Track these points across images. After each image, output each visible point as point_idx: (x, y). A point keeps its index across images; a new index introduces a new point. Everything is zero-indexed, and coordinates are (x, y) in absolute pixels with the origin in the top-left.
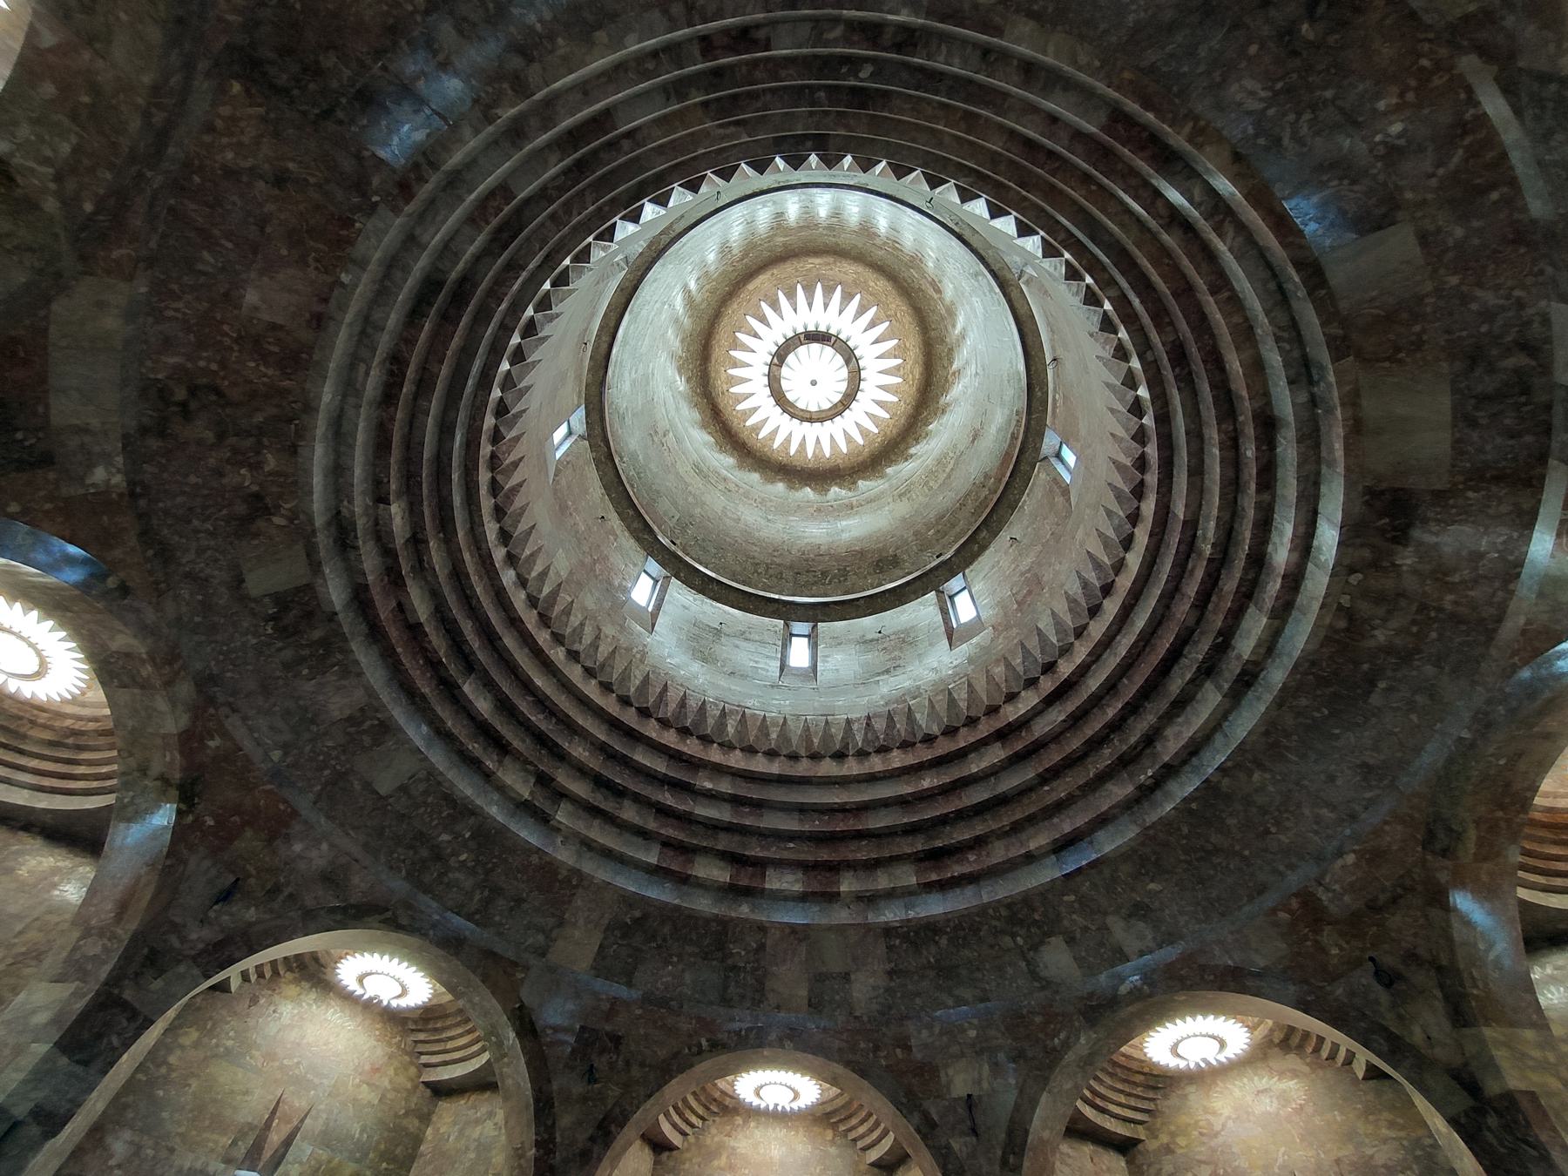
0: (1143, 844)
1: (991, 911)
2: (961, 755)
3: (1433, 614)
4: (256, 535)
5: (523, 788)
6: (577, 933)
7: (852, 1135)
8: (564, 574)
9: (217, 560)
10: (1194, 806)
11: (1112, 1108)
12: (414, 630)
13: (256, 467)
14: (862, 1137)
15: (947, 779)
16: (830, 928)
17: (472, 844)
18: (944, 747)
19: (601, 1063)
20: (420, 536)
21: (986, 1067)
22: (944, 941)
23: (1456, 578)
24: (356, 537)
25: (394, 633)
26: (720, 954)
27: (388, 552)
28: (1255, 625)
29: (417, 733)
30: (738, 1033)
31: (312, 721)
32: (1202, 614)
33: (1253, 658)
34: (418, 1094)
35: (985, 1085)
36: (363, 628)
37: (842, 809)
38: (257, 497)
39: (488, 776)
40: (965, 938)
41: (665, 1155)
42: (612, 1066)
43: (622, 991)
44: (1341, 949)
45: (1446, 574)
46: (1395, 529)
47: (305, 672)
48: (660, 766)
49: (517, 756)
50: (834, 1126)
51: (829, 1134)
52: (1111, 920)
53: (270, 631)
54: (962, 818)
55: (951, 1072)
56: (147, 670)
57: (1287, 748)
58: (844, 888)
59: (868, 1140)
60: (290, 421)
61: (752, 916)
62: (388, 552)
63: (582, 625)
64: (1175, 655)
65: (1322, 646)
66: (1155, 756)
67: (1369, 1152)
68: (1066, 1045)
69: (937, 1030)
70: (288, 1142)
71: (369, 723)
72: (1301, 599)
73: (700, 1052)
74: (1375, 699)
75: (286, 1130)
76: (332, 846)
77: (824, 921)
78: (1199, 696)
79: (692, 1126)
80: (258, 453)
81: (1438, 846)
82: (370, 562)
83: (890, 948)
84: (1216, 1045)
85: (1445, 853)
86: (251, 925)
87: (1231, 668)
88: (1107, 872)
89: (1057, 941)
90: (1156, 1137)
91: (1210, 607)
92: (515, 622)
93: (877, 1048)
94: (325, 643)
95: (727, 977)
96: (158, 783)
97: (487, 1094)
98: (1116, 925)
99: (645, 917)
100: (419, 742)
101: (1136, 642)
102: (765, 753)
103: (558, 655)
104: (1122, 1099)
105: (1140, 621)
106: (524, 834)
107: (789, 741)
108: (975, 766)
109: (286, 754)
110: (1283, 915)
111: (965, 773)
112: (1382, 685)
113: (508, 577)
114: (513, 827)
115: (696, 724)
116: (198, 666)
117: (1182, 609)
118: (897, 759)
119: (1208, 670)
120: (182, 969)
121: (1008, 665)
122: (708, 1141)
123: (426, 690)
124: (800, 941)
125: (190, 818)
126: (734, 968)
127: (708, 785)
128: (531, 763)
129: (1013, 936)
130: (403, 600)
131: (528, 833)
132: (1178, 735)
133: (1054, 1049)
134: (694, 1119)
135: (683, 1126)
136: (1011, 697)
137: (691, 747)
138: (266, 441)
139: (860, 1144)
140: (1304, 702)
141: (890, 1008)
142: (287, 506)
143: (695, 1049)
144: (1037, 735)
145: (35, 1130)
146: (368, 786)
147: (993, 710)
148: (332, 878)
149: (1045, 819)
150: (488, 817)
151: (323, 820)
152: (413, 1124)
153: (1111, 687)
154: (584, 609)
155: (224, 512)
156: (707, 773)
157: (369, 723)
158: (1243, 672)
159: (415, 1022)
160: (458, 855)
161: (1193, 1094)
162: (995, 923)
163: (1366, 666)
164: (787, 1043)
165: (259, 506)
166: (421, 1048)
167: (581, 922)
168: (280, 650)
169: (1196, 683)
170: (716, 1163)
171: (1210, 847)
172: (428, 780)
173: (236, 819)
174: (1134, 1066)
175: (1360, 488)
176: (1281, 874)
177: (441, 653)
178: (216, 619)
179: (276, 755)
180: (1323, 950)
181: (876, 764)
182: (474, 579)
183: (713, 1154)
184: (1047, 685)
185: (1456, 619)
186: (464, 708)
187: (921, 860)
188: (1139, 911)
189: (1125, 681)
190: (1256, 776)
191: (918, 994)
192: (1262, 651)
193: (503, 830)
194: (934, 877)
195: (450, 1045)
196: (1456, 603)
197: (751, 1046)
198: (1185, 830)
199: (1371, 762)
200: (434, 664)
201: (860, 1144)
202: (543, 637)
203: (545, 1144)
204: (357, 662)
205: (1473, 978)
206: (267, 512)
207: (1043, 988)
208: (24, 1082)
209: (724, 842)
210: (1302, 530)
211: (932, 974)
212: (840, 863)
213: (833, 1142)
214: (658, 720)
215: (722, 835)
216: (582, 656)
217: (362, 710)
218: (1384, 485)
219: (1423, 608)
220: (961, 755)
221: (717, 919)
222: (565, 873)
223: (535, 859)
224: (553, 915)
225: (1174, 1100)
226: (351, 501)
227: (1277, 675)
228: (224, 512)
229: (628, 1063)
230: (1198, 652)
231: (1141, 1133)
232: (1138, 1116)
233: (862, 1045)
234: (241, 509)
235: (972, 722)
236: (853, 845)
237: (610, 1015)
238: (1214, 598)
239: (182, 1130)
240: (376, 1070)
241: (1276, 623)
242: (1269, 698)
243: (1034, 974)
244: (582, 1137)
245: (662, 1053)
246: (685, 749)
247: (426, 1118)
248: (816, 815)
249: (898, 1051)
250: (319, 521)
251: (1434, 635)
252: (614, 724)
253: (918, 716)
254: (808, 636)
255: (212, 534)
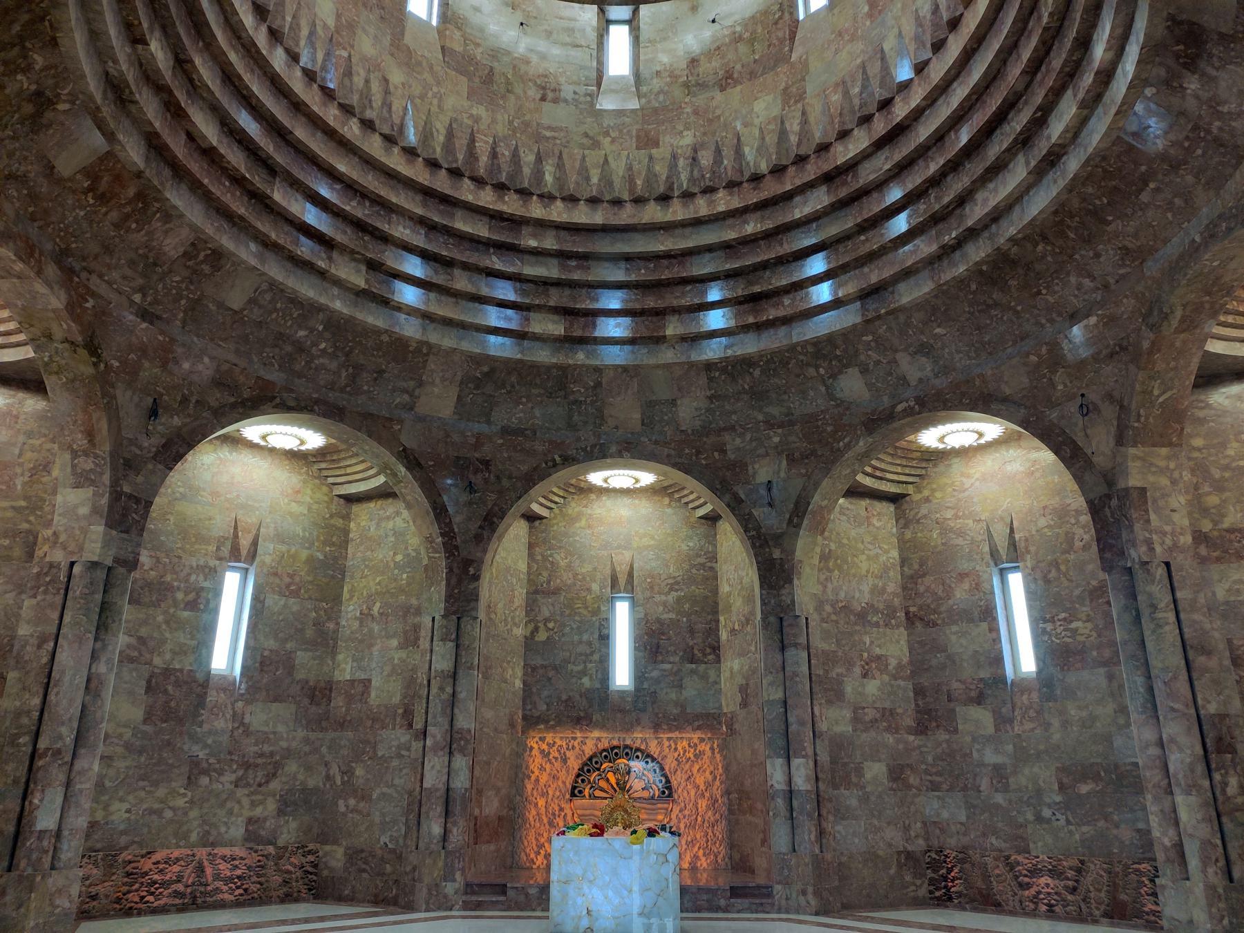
0: (936, 297)
1: (799, 349)
2: (788, 197)
3: (1202, 134)
4: (49, 126)
5: (357, 277)
6: (436, 390)
7: (684, 500)
8: (331, 22)
9: (26, 158)
10: (984, 268)
11: (889, 476)
12: (209, 154)
13: (27, 69)
14: (693, 501)
15: (769, 225)
16: (658, 366)
17: (327, 335)
18: (771, 188)
19: (477, 479)
20: (182, 56)
21: (785, 462)
22: (757, 372)
23: (1225, 109)
24: (131, 93)
25: (196, 166)
26: (562, 393)
27: (160, 89)
28: (1067, 110)
29: (247, 252)
30: (584, 450)
31: (155, 264)
32: (1031, 81)
33: (1060, 142)
34: (335, 503)
35: (782, 474)
36: (167, 172)
37: (668, 255)
38: (39, 93)
39: (322, 274)
40: (774, 370)
41: (537, 523)
42: (486, 481)
43: (484, 428)
44: (1065, 386)
45: (1218, 104)
46: (1186, 56)
47: (134, 226)
48: (481, 229)
49: (343, 249)
50: (670, 495)
51: (666, 501)
52: (899, 356)
53: (92, 201)
54: (782, 263)
55: (757, 466)
56: (19, 267)
57: (1069, 227)
58: (669, 332)
59: (697, 503)
60: (42, 19)
61: (588, 362)
62: (160, 89)
63: (367, 81)
64: (1000, 118)
65: (1114, 144)
66: (962, 218)
67: (1068, 501)
68: (848, 447)
69: (748, 437)
70: (255, 543)
71: (202, 255)
72: (1106, 98)
73: (555, 465)
74: (1145, 197)
75: (250, 538)
76: (212, 358)
77: (652, 361)
78: (1011, 166)
79: (556, 503)
80: (25, 57)
81: (1151, 321)
82: (150, 107)
83: (711, 379)
84: (976, 436)
85: (1152, 327)
86: (180, 428)
87: (1042, 147)
88: (902, 318)
89: (853, 372)
90: (920, 492)
91: (1039, 76)
92: (297, 106)
93: (698, 453)
94: (140, 196)
95: (571, 410)
96: (66, 345)
97: (390, 500)
98: (903, 360)
99: (493, 370)
100: (253, 262)
101: (969, 96)
102: (587, 200)
103: (352, 130)
104: (899, 470)
105: (977, 72)
106: (370, 320)
107: (610, 183)
108: (801, 209)
109: (144, 295)
110: (1033, 358)
111: (789, 219)
112: (1152, 185)
113: (278, 60)
114: (360, 316)
115: (511, 177)
116: (49, 246)
117: (1015, 72)
118: (723, 202)
119: (1024, 141)
120: (150, 466)
121: (846, 93)
122: (570, 512)
123: (242, 211)
124: (632, 377)
125: (102, 366)
126: (576, 402)
127: (533, 243)
128: (358, 253)
129: (817, 367)
130: (190, 129)
131: (373, 318)
132: (986, 200)
133: (839, 450)
134: (557, 499)
135: (549, 504)
136: (844, 135)
137: (511, 205)
138: (28, 45)
139: (691, 506)
140: (1090, 190)
141: (711, 423)
142: (65, 92)
143: (550, 464)
144: (861, 182)
145: (122, 570)
146: (221, 305)
147: (824, 148)
148: (219, 382)
149: (856, 268)
150: (333, 311)
151: (195, 339)
152: (339, 522)
153: (939, 137)
154: (364, 59)
155: (17, 116)
156: (530, 229)
157: (202, 255)
158: (1049, 153)
159: (314, 456)
160: (317, 345)
161: (957, 465)
162: (801, 357)
163: (1143, 168)
164: (625, 454)
165: (42, 101)
166: (325, 473)
167: (438, 381)
168: (106, 214)
169: (1011, 152)
170: (577, 525)
171: (991, 302)
172: (272, 290)
173: (132, 356)
174: (914, 447)
175: (1165, 14)
176: (1042, 326)
177: (243, 170)
178: (45, 204)
179: (137, 298)
180: (1054, 386)
181: (702, 207)
182: (247, 77)
183: (574, 520)
184: (880, 126)
185: (1219, 142)
186: (279, 214)
187: (740, 303)
188: (924, 350)
189: (952, 133)
190: (1040, 248)
191: (735, 413)
192: (1069, 135)
193: (350, 320)
194: (751, 320)
195: (349, 470)
196: (1220, 129)
197: (600, 454)
198: (974, 287)
199: (1130, 246)
200: (238, 181)
201: (691, 506)
202: (331, 115)
203: (448, 534)
204: (175, 207)
205: (1139, 415)
206: (51, 103)
207: (838, 406)
208: (103, 548)
209: (555, 298)
210: (1119, 31)
211: (746, 397)
212: (665, 309)
213: (669, 505)
214: (472, 179)
215: (553, 291)
216: (377, 122)
217: (193, 244)
218: (1184, 17)
219: (1196, 128)
220: (788, 197)
221: (556, 366)
222: (415, 345)
223: (385, 338)
224: (411, 379)
225: (941, 468)
226: (115, 61)
227: (1073, 164)
228: (17, 116)
229: (498, 477)
230: (1018, 122)
231: (910, 489)
232: (911, 479)
233: (687, 451)
234: (28, 109)
235: (801, 160)
236: (678, 290)
237: (478, 445)
238: (1043, 68)
239: (179, 545)
240: (298, 492)
241: (1085, 112)
242: (1062, 183)
243: (831, 396)
244: (474, 527)
245: (524, 468)
246: (505, 208)
247: (347, 517)
248: (641, 263)
249: (716, 454)
250: (98, 98)
251: (1199, 152)
252: (428, 193)
253: (747, 150)
254: (628, 22)
255: (14, 138)
